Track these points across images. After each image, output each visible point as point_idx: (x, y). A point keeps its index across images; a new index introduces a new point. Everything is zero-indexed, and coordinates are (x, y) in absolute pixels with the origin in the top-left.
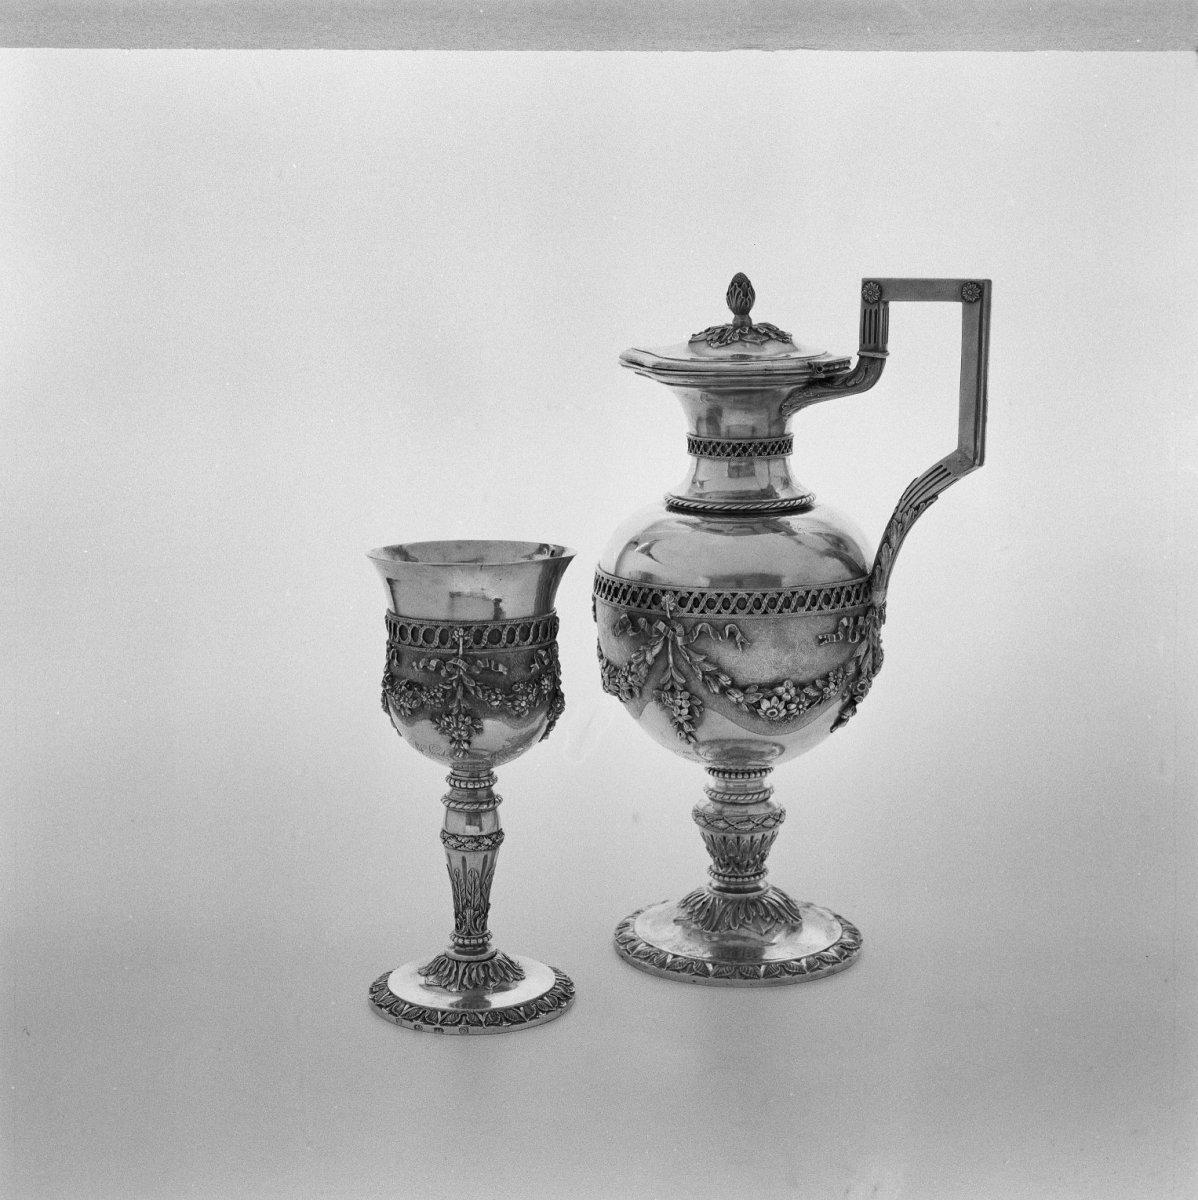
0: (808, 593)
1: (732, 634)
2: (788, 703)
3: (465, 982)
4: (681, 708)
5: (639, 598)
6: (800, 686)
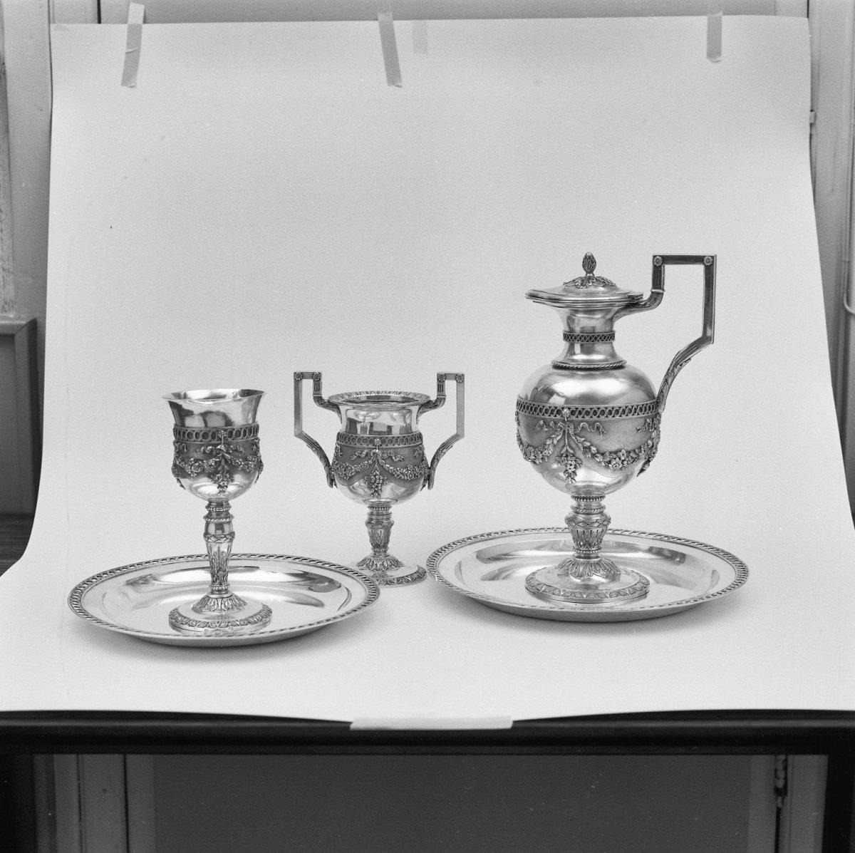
0: (632, 407)
1: (598, 428)
2: (623, 461)
3: (223, 607)
4: (571, 465)
5: (550, 412)
6: (629, 452)
